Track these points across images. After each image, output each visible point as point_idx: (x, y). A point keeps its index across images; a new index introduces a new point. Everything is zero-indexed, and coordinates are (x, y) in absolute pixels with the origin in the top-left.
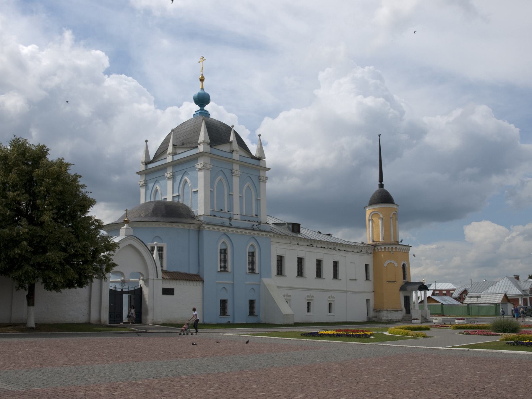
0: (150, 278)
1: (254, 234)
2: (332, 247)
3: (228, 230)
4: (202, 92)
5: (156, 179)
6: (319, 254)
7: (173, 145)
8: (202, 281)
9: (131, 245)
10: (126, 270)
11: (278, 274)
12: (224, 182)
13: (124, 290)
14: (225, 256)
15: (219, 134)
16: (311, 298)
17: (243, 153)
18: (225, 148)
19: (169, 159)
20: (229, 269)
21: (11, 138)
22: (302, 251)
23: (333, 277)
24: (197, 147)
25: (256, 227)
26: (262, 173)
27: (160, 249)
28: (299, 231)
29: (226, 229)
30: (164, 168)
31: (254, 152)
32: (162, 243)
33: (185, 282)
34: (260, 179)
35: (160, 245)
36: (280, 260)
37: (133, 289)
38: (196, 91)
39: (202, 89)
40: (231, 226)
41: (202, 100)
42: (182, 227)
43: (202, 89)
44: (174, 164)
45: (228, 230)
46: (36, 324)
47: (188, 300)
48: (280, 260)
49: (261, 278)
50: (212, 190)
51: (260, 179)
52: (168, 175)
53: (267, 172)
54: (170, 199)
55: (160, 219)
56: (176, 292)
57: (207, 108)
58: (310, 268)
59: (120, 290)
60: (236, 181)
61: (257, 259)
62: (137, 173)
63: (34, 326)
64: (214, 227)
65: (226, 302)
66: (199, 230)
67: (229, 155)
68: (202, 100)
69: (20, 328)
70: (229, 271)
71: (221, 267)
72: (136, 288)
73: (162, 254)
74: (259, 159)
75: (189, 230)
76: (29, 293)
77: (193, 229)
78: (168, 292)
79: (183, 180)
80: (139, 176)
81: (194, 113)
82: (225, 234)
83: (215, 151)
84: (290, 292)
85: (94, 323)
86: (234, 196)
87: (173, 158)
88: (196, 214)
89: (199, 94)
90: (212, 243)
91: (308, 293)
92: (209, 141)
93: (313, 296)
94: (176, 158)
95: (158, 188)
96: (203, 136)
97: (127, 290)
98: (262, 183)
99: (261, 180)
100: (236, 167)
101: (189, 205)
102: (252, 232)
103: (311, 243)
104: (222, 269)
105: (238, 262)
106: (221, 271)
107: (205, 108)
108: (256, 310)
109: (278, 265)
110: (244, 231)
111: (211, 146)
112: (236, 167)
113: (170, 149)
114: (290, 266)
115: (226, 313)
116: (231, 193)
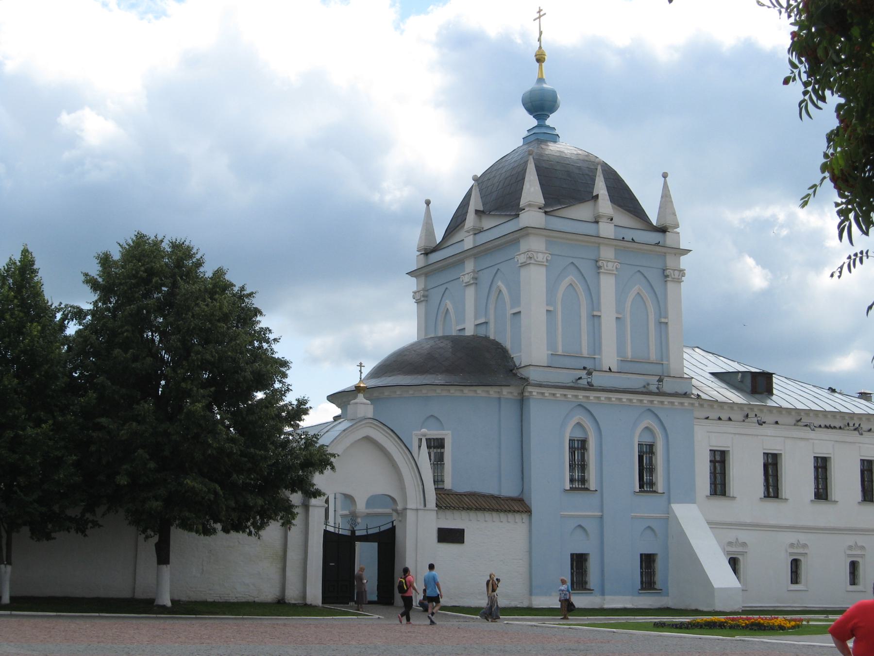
0: (409, 506)
1: (652, 402)
2: (713, 415)
3: (588, 397)
4: (538, 86)
5: (444, 286)
6: (823, 443)
7: (477, 212)
8: (528, 511)
9: (368, 439)
10: (349, 488)
11: (767, 496)
12: (580, 288)
13: (358, 533)
14: (583, 455)
15: (570, 183)
16: (801, 551)
17: (624, 219)
18: (582, 211)
19: (469, 243)
20: (592, 484)
21: (128, 237)
22: (772, 439)
23: (859, 495)
24: (517, 216)
25: (653, 388)
26: (670, 262)
27: (436, 445)
28: (769, 391)
29: (581, 394)
30: (457, 261)
31: (653, 217)
32: (443, 430)
33: (488, 515)
34: (667, 276)
35: (435, 434)
36: (719, 461)
37: (376, 530)
38: (530, 84)
39: (541, 80)
40: (590, 387)
41: (540, 105)
42: (484, 394)
43: (541, 80)
44: (479, 252)
45: (588, 397)
46: (172, 601)
47: (493, 555)
48: (719, 461)
49: (669, 503)
50: (551, 309)
51: (667, 276)
52: (467, 279)
53: (682, 258)
54: (469, 332)
55: (439, 379)
56: (434, 535)
57: (551, 121)
58: (797, 477)
59: (348, 533)
60: (608, 285)
61: (660, 460)
62: (714, 374)
63: (169, 604)
64: (553, 391)
65: (586, 560)
66: (522, 401)
67: (590, 229)
68: (540, 105)
69: (143, 606)
70: (660, 490)
71: (572, 480)
72: (383, 529)
73: (442, 454)
74: (663, 230)
75: (499, 398)
76: (160, 537)
77: (510, 396)
78: (451, 536)
79: (494, 288)
80: (414, 279)
81: (526, 134)
82: (649, 410)
83: (556, 223)
84: (743, 536)
85: (293, 602)
86: (604, 319)
87: (474, 241)
88: (517, 364)
89: (532, 92)
90: (551, 428)
91: (850, 540)
92: (541, 200)
93: (805, 546)
94: (483, 238)
95: (450, 306)
96: (532, 191)
97: (364, 533)
98: (670, 286)
99: (670, 276)
100: (607, 253)
101: (508, 345)
102: (646, 399)
103: (801, 419)
104: (576, 485)
105: (614, 467)
106: (572, 489)
107: (549, 122)
108: (659, 578)
109: (816, 478)
110: (625, 397)
111: (546, 213)
112: (607, 253)
113: (471, 220)
114: (746, 474)
115: (586, 583)
116: (663, 320)
